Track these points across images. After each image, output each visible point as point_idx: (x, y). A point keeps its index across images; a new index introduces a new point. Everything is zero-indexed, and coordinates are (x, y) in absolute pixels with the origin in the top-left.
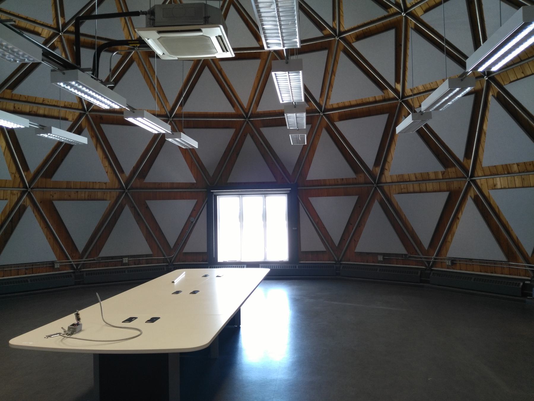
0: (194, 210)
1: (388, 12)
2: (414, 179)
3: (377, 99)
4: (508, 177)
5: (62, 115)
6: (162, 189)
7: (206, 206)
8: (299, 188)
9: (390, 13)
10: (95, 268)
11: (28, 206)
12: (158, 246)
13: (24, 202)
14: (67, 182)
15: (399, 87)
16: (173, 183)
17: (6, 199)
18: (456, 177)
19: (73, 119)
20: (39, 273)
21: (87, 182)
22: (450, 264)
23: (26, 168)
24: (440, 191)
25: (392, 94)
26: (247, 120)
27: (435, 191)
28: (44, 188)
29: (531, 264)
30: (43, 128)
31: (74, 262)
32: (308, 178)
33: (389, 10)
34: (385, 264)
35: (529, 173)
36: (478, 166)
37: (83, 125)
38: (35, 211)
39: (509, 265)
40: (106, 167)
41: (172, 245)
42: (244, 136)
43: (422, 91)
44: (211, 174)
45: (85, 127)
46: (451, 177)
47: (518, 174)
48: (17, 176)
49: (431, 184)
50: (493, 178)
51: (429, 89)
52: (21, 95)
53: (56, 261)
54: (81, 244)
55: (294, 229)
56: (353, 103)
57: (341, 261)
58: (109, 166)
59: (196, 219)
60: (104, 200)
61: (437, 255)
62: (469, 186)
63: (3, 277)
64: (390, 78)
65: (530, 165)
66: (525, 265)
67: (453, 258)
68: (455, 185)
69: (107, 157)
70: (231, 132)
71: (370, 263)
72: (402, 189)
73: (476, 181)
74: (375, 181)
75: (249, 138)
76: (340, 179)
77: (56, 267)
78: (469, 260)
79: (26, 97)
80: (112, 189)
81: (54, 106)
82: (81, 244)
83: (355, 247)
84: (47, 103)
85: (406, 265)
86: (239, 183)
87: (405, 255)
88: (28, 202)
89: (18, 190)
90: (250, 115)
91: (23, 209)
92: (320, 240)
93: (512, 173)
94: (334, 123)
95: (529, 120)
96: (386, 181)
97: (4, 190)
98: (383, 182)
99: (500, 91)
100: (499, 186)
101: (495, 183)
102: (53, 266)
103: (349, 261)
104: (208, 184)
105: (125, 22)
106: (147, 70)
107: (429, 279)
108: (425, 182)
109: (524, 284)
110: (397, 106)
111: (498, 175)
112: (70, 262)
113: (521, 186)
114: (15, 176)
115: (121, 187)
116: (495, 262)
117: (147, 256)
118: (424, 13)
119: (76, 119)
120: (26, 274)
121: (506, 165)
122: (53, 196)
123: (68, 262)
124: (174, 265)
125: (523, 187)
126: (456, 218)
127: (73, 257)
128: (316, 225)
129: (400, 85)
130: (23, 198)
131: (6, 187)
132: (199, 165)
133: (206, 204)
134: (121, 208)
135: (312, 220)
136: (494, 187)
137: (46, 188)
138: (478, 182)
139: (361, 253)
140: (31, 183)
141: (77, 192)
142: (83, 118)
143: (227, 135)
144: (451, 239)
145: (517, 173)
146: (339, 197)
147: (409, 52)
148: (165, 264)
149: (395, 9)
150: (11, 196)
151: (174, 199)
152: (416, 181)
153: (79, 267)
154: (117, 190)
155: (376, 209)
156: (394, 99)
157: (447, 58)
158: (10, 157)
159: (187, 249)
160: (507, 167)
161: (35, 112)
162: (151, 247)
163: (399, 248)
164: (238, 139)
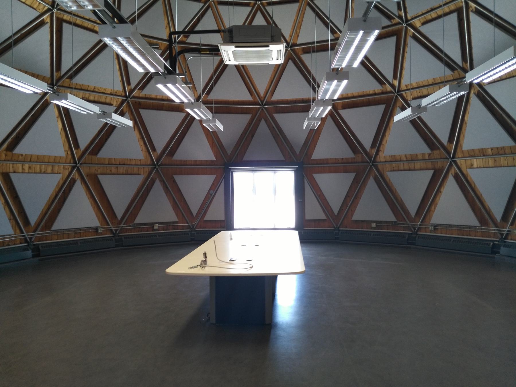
0: (213, 184)
1: (392, 22)
2: (405, 159)
3: (377, 92)
4: (483, 159)
5: (108, 101)
6: (187, 165)
7: (223, 181)
8: (304, 166)
9: (393, 23)
10: (130, 233)
11: (77, 179)
12: (183, 214)
13: (74, 175)
14: (109, 158)
15: (396, 83)
16: (196, 161)
17: (60, 173)
18: (440, 158)
19: (117, 105)
20: (85, 237)
21: (125, 159)
22: (432, 229)
23: (77, 146)
24: (426, 169)
25: (389, 88)
26: (262, 107)
27: (422, 170)
28: (89, 164)
29: (500, 228)
30: (104, 113)
31: (113, 227)
32: (313, 158)
33: (392, 21)
34: (377, 229)
35: (500, 156)
36: (458, 150)
37: (125, 110)
38: (82, 183)
39: (482, 229)
40: (141, 146)
41: (195, 214)
42: (259, 121)
43: (415, 87)
44: (229, 152)
45: (126, 112)
46: (435, 157)
47: (492, 157)
48: (69, 153)
49: (418, 164)
50: (471, 159)
51: (421, 85)
52: (77, 84)
53: (99, 227)
54: (119, 212)
55: (299, 200)
56: (356, 94)
57: (339, 228)
58: (144, 145)
59: (215, 192)
60: (138, 174)
61: (422, 222)
62: (451, 165)
63: (57, 240)
64: (389, 74)
65: (502, 149)
66: (494, 229)
67: (435, 224)
68: (439, 165)
69: (142, 138)
70: (248, 117)
71: (364, 229)
72: (393, 167)
73: (456, 162)
74: (371, 160)
75: (263, 123)
76: (341, 158)
77: (99, 232)
78: (448, 226)
79: (81, 85)
80: (145, 165)
81: (103, 93)
82: (119, 212)
83: (352, 215)
84: (97, 90)
85: (395, 230)
86: (252, 161)
87: (395, 222)
88: (77, 176)
89: (69, 166)
90: (265, 103)
91: (73, 181)
92: (321, 210)
93: (487, 156)
94: (338, 111)
95: (502, 114)
96: (380, 160)
97: (58, 165)
98: (378, 161)
99: (480, 90)
100: (475, 166)
101: (472, 163)
102: (97, 231)
103: (346, 227)
104: (226, 162)
105: (167, 22)
106: (181, 63)
107: (415, 242)
108: (414, 162)
109: (494, 244)
110: (393, 98)
111: (475, 156)
112: (110, 228)
113: (493, 166)
114: (67, 153)
115: (153, 164)
116: (470, 227)
117: (173, 223)
118: (421, 25)
119: (119, 105)
120: (75, 237)
121: (482, 149)
122: (97, 171)
123: (108, 228)
124: (196, 231)
125: (495, 167)
126: (439, 191)
127: (112, 224)
128: (318, 198)
129: (397, 81)
130: (73, 173)
131: (60, 162)
132: (219, 144)
133: (224, 179)
134: (153, 182)
135: (315, 193)
136: (471, 167)
137: (91, 164)
138: (458, 162)
139: (356, 221)
140: (80, 159)
141: (117, 167)
142: (125, 103)
143: (243, 120)
144: (434, 208)
145: (490, 156)
146: (340, 174)
147: (407, 55)
148: (188, 230)
149: (397, 20)
150: (64, 171)
151: (197, 174)
152: (406, 161)
153: (118, 232)
154: (149, 166)
155: (371, 183)
156: (391, 92)
157: (445, 67)
158: (65, 137)
159: (208, 217)
160: (483, 151)
161: (87, 98)
162: (177, 215)
163: (390, 217)
164: (253, 124)
